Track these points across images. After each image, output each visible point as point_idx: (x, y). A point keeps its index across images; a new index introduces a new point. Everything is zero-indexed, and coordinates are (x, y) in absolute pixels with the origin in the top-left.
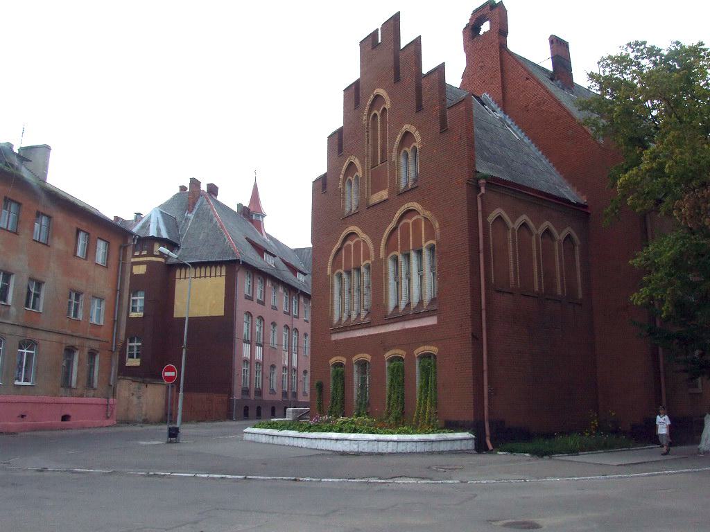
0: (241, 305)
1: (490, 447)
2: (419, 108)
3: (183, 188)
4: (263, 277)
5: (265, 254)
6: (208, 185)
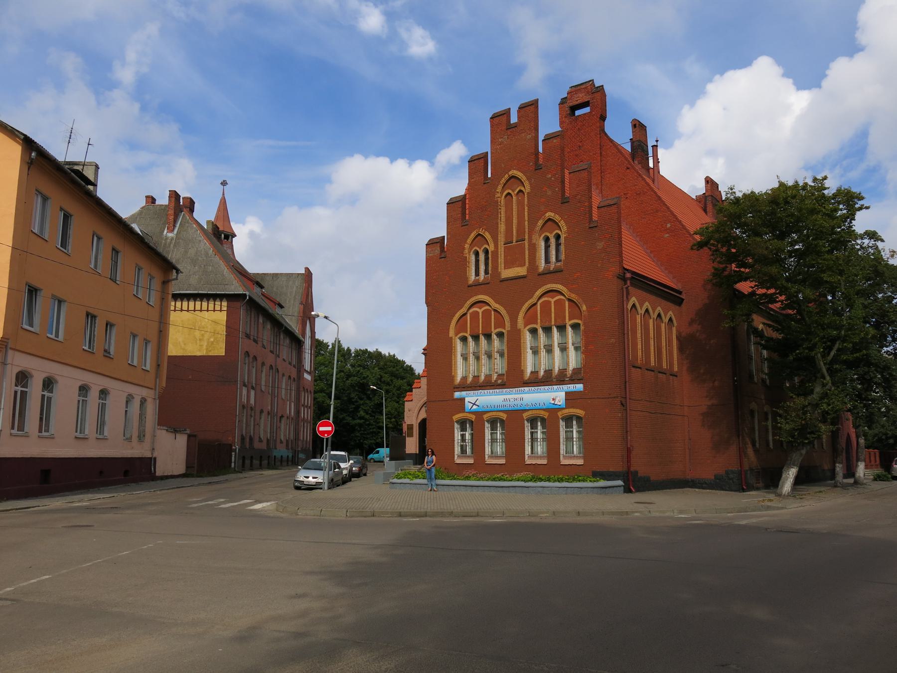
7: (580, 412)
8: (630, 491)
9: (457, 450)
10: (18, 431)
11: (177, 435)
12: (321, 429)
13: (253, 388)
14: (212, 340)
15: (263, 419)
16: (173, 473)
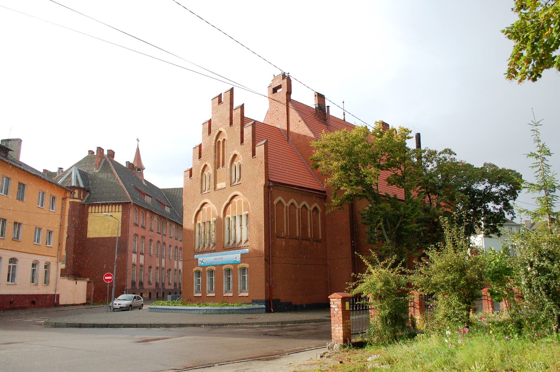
0: (133, 230)
1: (272, 311)
2: (242, 141)
3: (91, 152)
4: (145, 211)
5: (146, 196)
6: (108, 150)
7: (247, 265)
8: (270, 312)
9: (195, 288)
10: (11, 282)
11: (78, 282)
12: (106, 278)
13: (142, 254)
14: (114, 228)
15: (151, 272)
16: (74, 302)
